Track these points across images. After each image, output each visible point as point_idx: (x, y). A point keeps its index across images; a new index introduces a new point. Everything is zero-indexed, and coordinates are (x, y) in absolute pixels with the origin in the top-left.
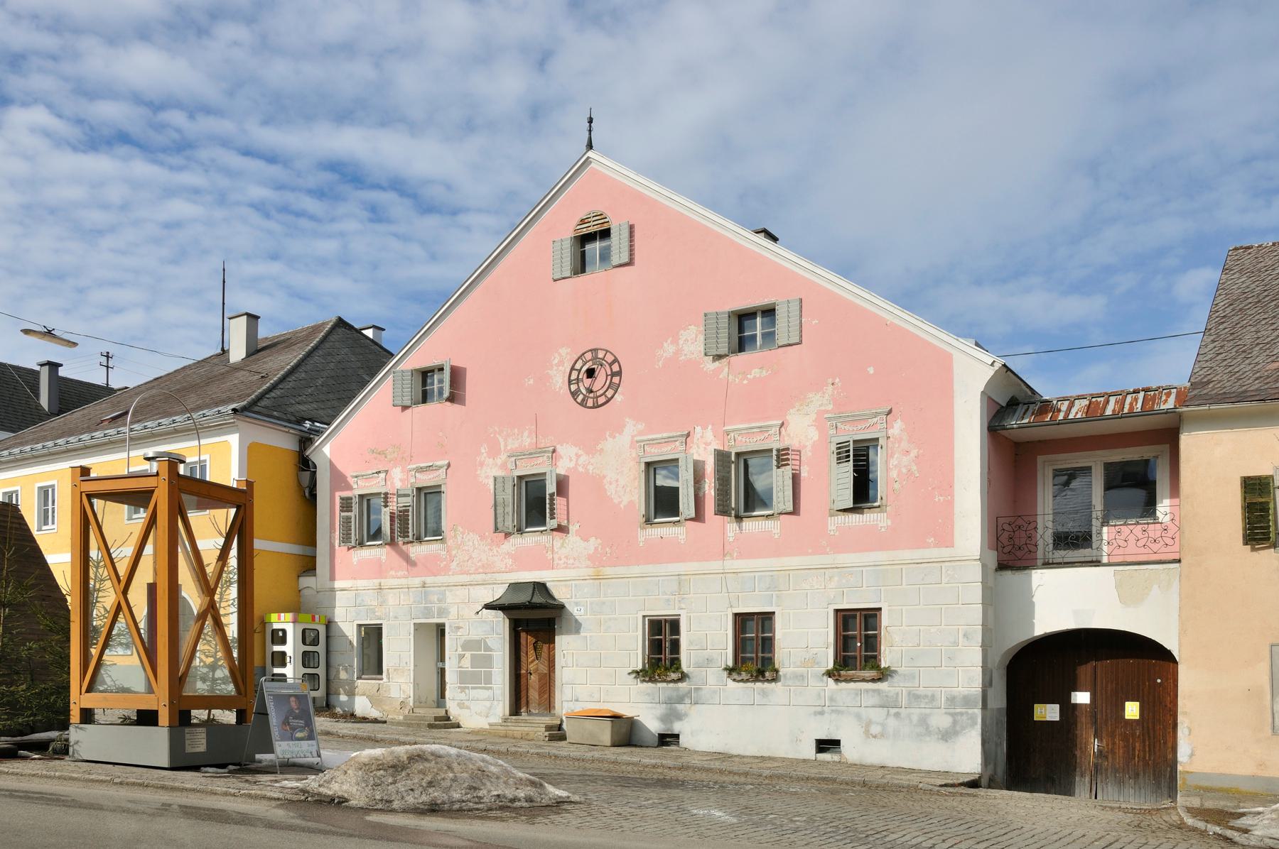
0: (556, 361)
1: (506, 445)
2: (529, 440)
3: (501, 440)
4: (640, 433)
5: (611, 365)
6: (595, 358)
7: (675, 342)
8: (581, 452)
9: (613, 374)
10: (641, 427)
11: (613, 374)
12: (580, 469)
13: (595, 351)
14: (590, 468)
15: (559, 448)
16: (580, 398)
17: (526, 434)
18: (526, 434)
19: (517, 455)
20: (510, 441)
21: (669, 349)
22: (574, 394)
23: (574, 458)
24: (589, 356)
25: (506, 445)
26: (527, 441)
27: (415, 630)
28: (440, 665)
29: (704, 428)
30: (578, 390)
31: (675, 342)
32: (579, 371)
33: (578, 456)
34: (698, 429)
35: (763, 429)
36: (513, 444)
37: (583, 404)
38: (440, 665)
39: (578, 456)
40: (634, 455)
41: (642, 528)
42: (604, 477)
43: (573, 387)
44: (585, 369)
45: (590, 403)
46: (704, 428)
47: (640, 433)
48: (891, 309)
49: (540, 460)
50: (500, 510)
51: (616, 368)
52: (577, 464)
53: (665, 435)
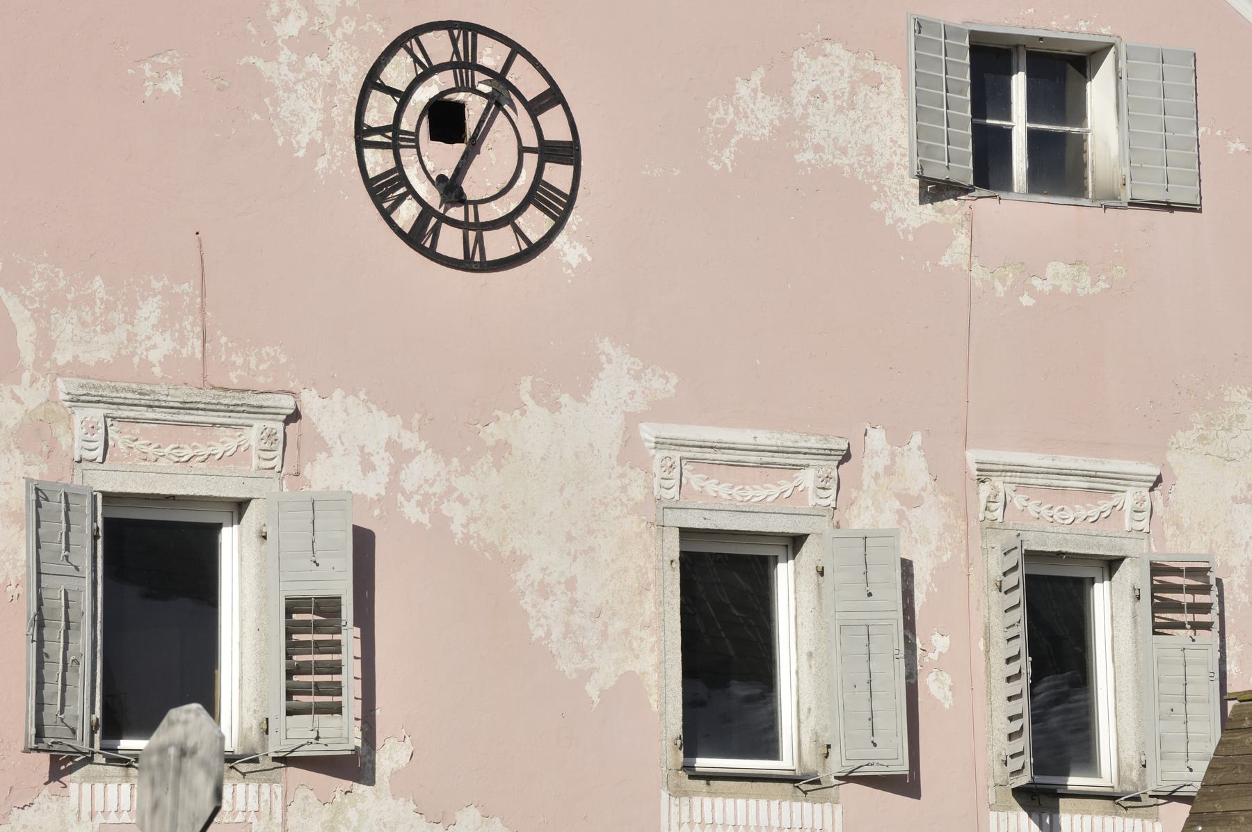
0: (291, 27)
1: (46, 344)
2: (163, 345)
3: (19, 315)
4: (659, 411)
5: (535, 108)
6: (465, 65)
7: (779, 87)
8: (410, 440)
9: (551, 152)
10: (664, 385)
11: (551, 152)
12: (412, 512)
13: (468, 31)
14: (456, 513)
15: (311, 403)
16: (407, 214)
17: (150, 310)
18: (150, 310)
19: (123, 402)
20: (65, 327)
21: (756, 112)
22: (385, 191)
23: (383, 463)
24: (439, 47)
25: (46, 344)
26: (155, 343)
27: (986, 187)
28: (266, 763)
29: (898, 438)
30: (397, 178)
31: (779, 87)
32: (404, 98)
33: (400, 456)
34: (877, 438)
35: (1101, 484)
36: (85, 345)
37: (418, 238)
38: (266, 763)
39: (400, 456)
40: (637, 493)
41: (677, 792)
42: (518, 560)
43: (378, 161)
44: (424, 95)
45: (450, 242)
46: (898, 438)
47: (659, 411)
48: (99, 637)
49: (225, 442)
50: (55, 636)
51: (554, 126)
52: (394, 484)
53: (765, 438)
